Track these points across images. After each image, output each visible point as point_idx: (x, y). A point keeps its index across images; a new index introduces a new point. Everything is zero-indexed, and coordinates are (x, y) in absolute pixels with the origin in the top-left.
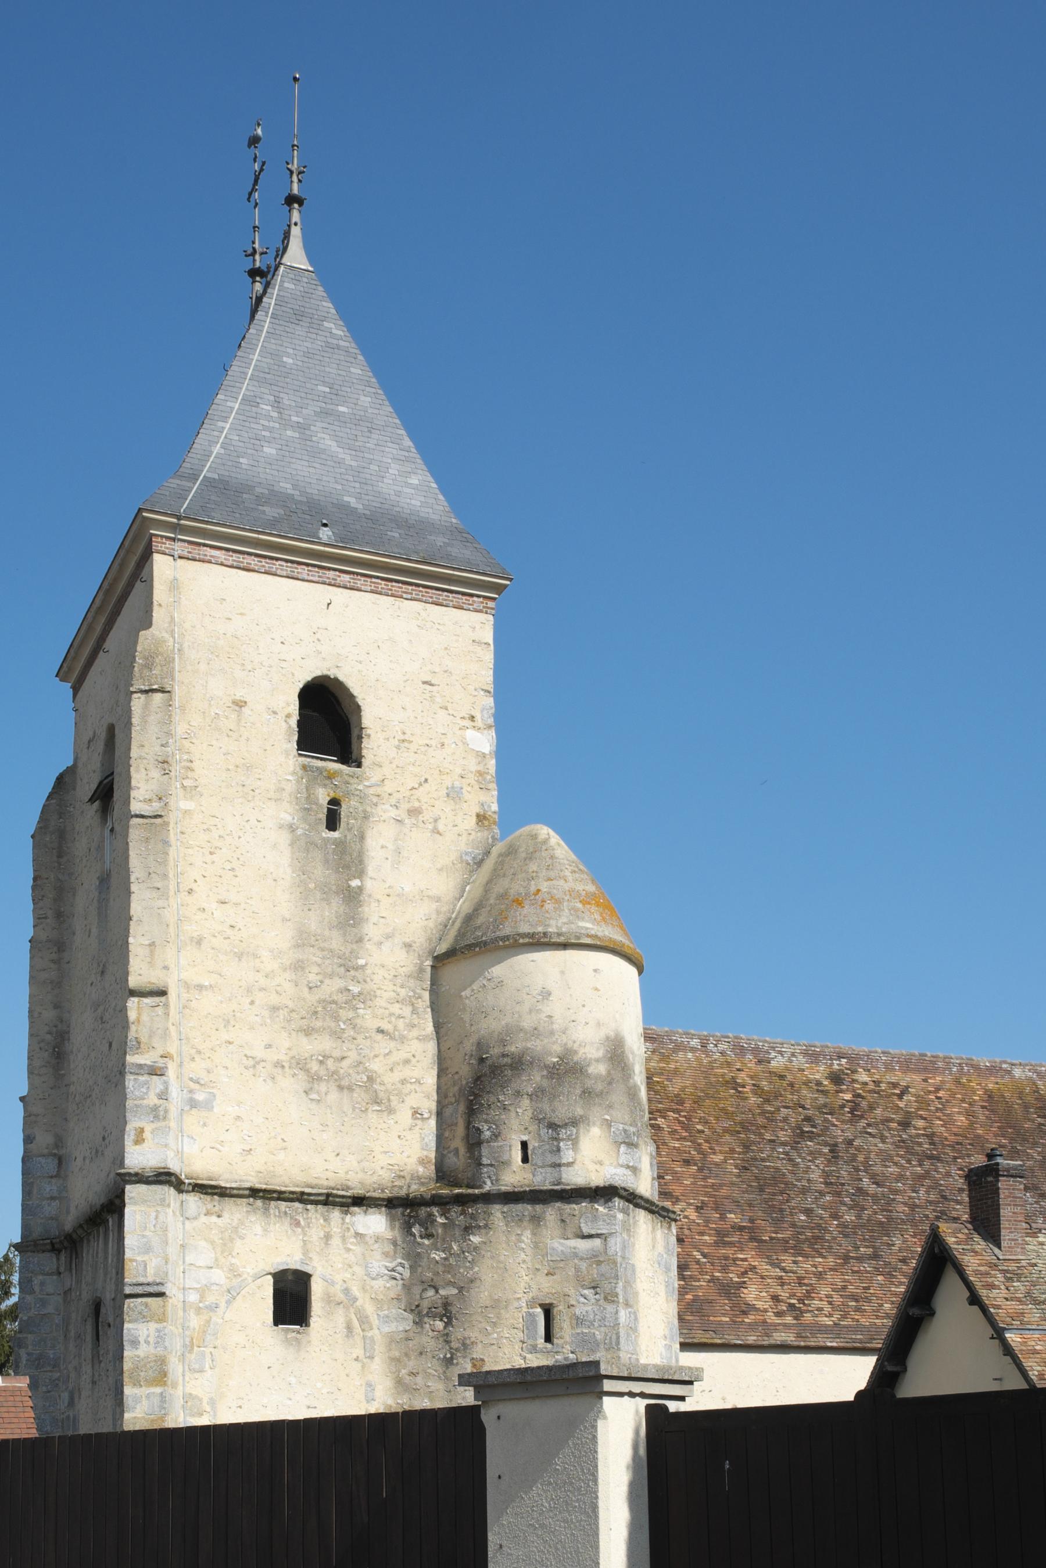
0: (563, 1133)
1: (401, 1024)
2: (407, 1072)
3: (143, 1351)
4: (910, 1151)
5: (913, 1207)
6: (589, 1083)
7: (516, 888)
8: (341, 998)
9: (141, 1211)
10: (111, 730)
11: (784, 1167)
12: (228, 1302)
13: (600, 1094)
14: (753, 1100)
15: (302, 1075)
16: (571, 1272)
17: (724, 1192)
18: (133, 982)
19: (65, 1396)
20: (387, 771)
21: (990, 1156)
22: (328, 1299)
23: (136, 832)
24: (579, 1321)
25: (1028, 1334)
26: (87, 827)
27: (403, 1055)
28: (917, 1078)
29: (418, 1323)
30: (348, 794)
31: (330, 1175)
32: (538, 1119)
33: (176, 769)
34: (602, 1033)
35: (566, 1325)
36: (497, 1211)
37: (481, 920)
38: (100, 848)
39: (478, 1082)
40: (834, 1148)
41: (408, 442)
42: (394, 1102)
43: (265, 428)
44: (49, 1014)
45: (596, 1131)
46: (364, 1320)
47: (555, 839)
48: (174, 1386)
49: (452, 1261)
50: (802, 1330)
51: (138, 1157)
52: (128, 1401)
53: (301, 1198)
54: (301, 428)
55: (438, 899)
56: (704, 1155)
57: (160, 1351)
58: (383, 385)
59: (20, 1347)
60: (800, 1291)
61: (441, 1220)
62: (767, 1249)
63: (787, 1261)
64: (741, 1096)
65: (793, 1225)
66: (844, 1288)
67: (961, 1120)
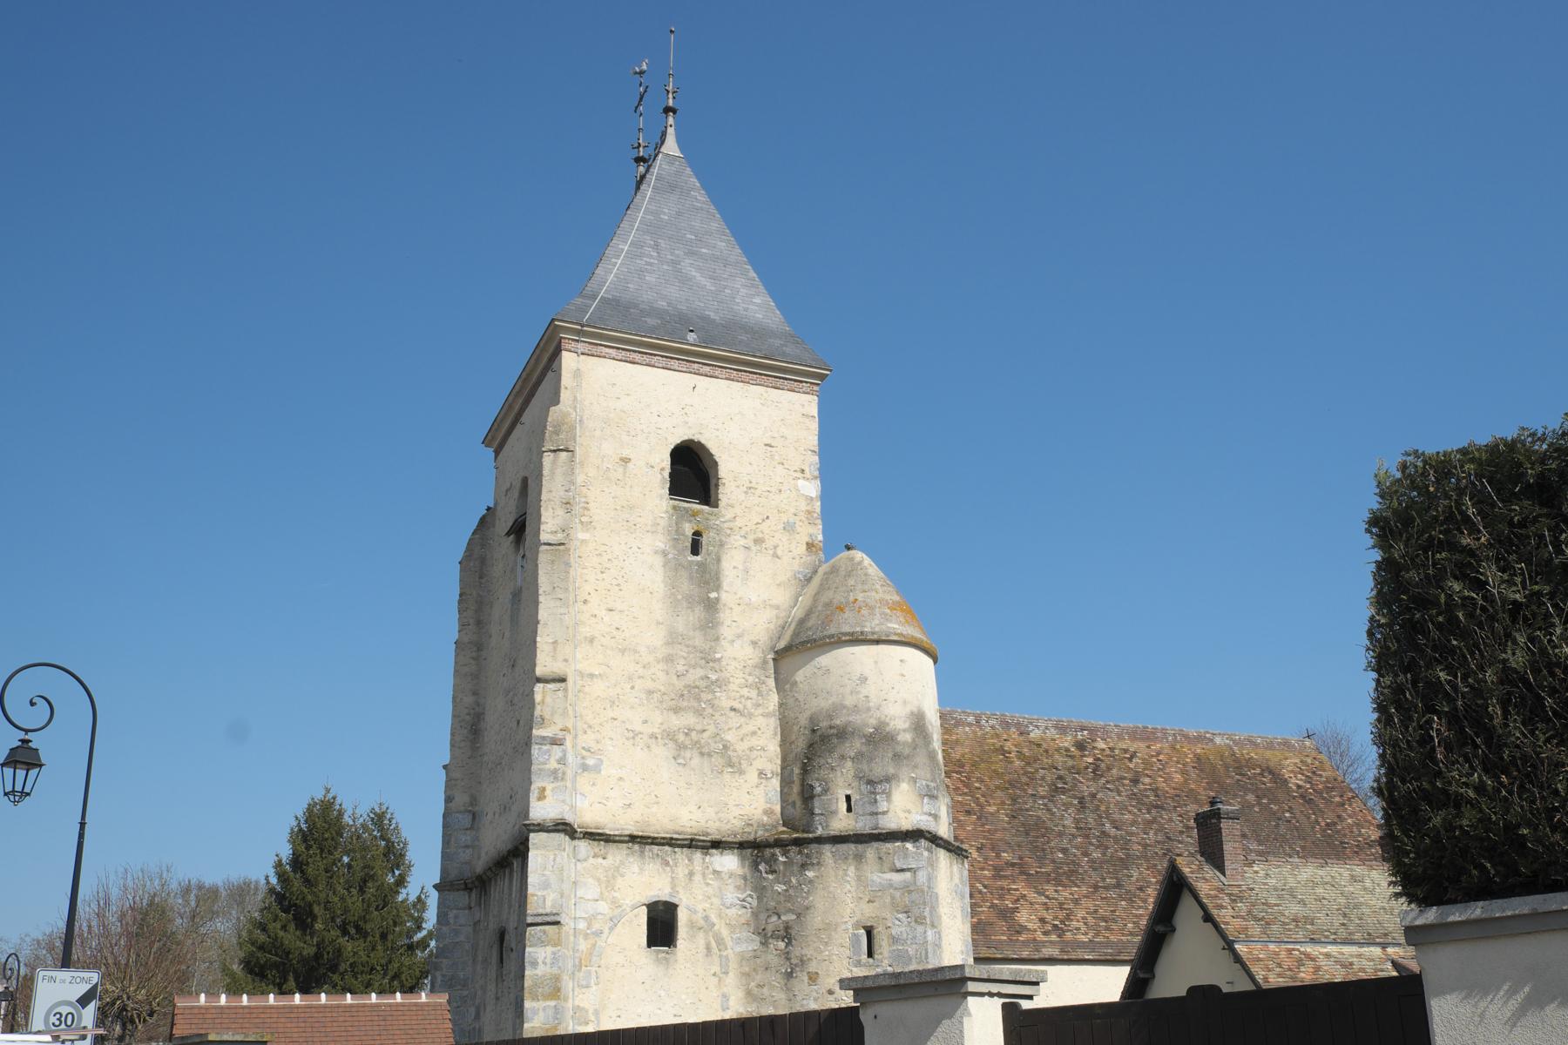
0: (879, 788)
1: (749, 703)
2: (754, 742)
3: (541, 970)
4: (1140, 801)
5: (1145, 846)
6: (899, 749)
7: (839, 598)
8: (703, 684)
9: (543, 857)
10: (525, 481)
11: (1045, 816)
12: (611, 929)
13: (907, 757)
14: (1017, 763)
15: (671, 745)
16: (888, 900)
17: (998, 835)
18: (539, 671)
19: (472, 1010)
20: (738, 510)
21: (1212, 803)
22: (692, 925)
23: (544, 557)
24: (895, 940)
25: (1253, 945)
26: (503, 557)
27: (751, 728)
28: (1142, 745)
29: (764, 944)
30: (708, 528)
31: (693, 823)
32: (859, 777)
33: (577, 509)
34: (908, 709)
35: (885, 943)
36: (827, 849)
37: (810, 624)
38: (513, 570)
39: (811, 750)
40: (1082, 800)
41: (753, 274)
42: (744, 765)
43: (648, 264)
44: (469, 700)
45: (904, 786)
46: (720, 942)
47: (867, 561)
48: (566, 1000)
49: (791, 892)
50: (1064, 946)
51: (541, 811)
52: (528, 1013)
53: (671, 842)
54: (674, 263)
55: (777, 607)
56: (981, 806)
57: (555, 970)
58: (734, 234)
59: (436, 969)
60: (1062, 915)
61: (782, 859)
62: (1033, 880)
63: (1050, 889)
64: (1008, 761)
65: (1053, 861)
66: (1096, 911)
67: (1178, 777)
